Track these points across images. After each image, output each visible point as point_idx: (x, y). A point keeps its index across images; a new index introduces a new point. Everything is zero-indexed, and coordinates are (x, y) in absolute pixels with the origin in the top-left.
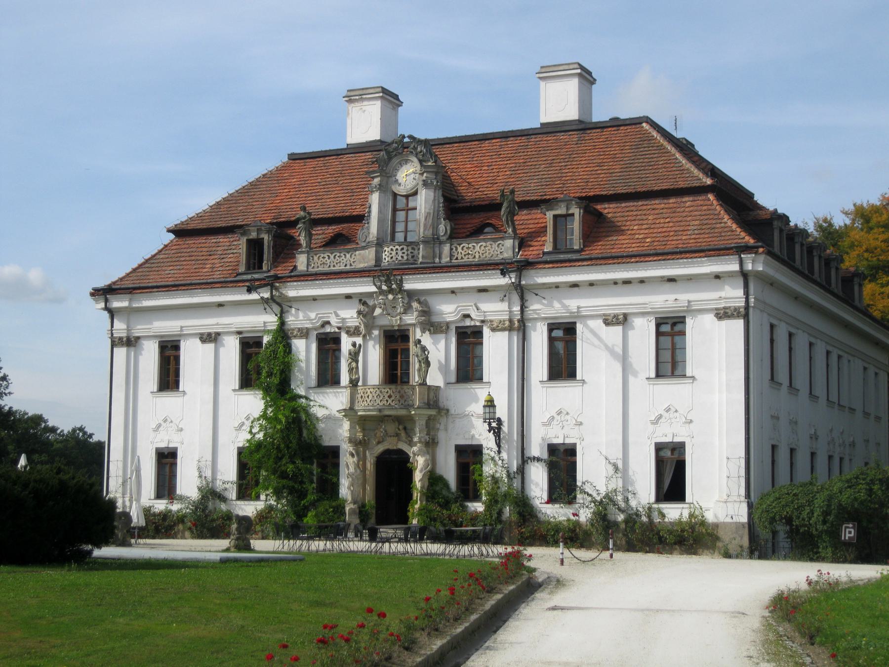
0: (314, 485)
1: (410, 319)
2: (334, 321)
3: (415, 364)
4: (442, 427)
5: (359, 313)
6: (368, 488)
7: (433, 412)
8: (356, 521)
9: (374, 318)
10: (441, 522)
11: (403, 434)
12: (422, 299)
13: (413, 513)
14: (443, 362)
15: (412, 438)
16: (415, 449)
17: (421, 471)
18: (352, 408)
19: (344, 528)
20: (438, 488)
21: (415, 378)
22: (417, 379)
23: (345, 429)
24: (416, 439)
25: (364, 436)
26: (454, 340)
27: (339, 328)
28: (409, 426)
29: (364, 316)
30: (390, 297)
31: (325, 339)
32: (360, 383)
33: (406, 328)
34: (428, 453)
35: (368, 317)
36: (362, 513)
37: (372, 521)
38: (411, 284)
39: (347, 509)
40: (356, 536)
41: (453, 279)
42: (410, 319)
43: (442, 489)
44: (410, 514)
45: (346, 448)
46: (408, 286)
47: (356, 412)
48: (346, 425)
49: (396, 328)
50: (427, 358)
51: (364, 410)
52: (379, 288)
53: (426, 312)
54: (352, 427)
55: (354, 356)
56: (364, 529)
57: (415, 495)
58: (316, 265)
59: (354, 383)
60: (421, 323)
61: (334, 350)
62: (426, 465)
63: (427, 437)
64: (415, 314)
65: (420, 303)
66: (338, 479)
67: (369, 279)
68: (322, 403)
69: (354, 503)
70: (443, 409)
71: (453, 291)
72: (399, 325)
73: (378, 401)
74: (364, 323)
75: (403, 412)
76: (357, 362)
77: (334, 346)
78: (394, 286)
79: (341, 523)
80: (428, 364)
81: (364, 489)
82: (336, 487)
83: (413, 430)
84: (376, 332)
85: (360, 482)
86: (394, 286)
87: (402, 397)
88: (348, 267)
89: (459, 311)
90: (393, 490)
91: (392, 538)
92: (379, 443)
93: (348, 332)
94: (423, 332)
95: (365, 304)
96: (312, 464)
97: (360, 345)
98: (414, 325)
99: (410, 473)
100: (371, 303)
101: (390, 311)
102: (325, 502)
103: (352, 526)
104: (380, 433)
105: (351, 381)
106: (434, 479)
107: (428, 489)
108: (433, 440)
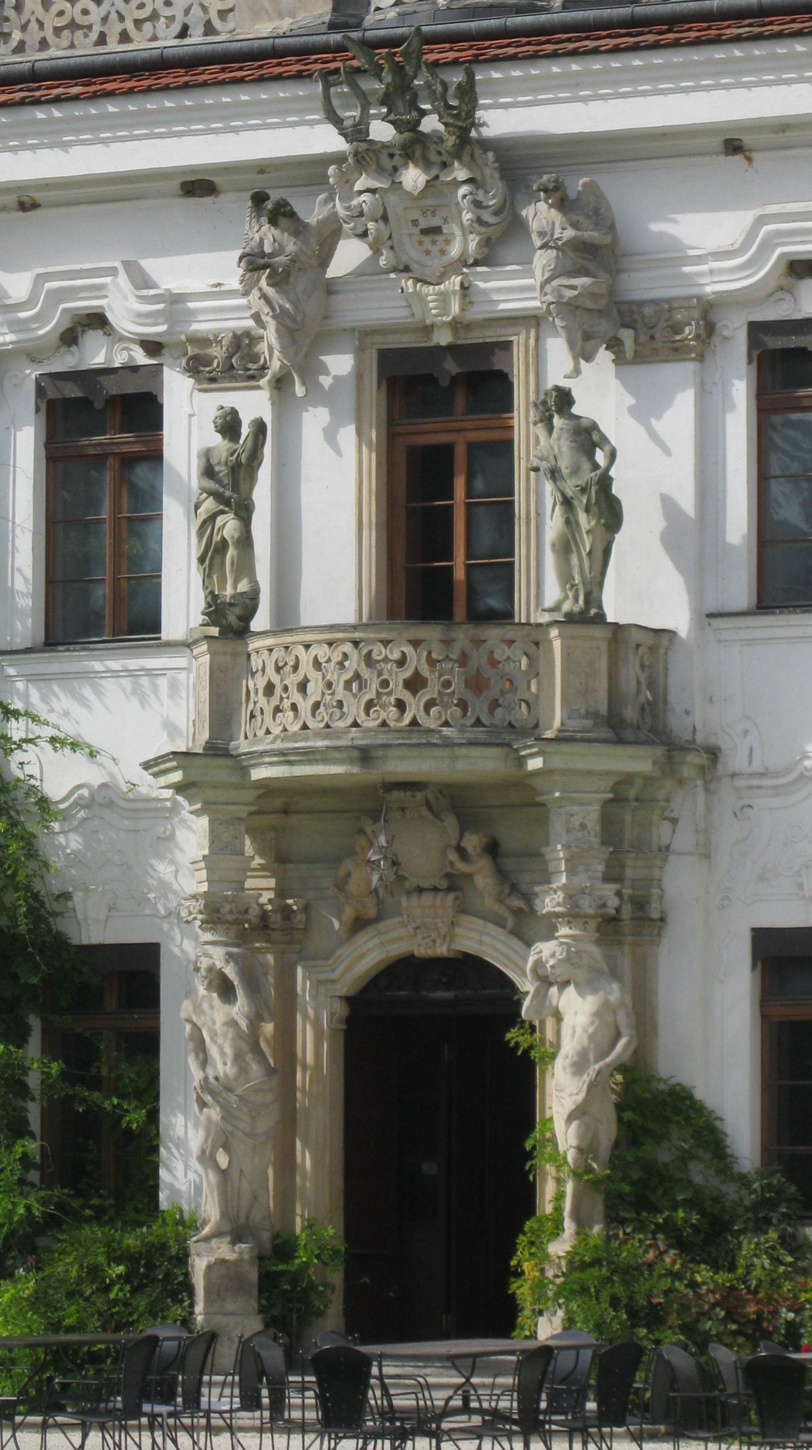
0: (33, 1146)
1: (517, 288)
2: (125, 309)
3: (541, 516)
4: (684, 839)
5: (255, 262)
6: (305, 1159)
7: (637, 761)
8: (243, 1321)
9: (330, 288)
10: (688, 1329)
11: (483, 878)
12: (577, 184)
13: (540, 1285)
14: (687, 503)
15: (529, 898)
16: (547, 951)
17: (579, 1066)
18: (217, 749)
19: (178, 1361)
20: (664, 1155)
21: (543, 588)
22: (552, 592)
23: (185, 857)
24: (551, 902)
25: (281, 892)
26: (740, 392)
27: (153, 347)
28: (512, 838)
29: (279, 280)
30: (413, 177)
31: (83, 404)
32: (261, 621)
33: (492, 335)
34: (615, 974)
35: (301, 284)
36: (276, 1284)
37: (327, 1331)
38: (521, 110)
39: (199, 1265)
40: (250, 1402)
41: (734, 76)
42: (517, 288)
43: (685, 1157)
44: (522, 1290)
45: (192, 952)
46: (499, 121)
47: (240, 765)
48: (193, 835)
49: (443, 338)
50: (605, 482)
51: (285, 757)
52: (356, 133)
53: (596, 252)
54: (221, 847)
55: (230, 482)
56: (293, 1363)
57: (547, 1191)
58: (34, 35)
59: (229, 621)
60: (570, 309)
61: (129, 461)
62: (606, 1034)
63: (608, 891)
64: (543, 260)
65: (563, 204)
66: (153, 1116)
67: (301, 90)
68: (68, 729)
69: (237, 1237)
70: (688, 747)
71: (734, 144)
72: (456, 325)
73: (354, 709)
74: (280, 316)
75: (484, 764)
76: (244, 511)
77: (126, 440)
78: (431, 124)
79: (167, 1333)
80: (610, 513)
81: (287, 1165)
82: (136, 1157)
83: (535, 856)
84: (340, 364)
85: (266, 1123)
86: (431, 124)
87: (477, 684)
88: (196, 38)
89: (767, 245)
90: (429, 1168)
91: (447, 1412)
92: (359, 924)
93: (197, 367)
94: (583, 352)
95: (282, 214)
96: (20, 1037)
97: (260, 428)
98: (531, 321)
99: (518, 1080)
100: (313, 212)
101: (412, 253)
102: (93, 1232)
103: (226, 1353)
104: (368, 876)
105: (216, 610)
106: (649, 1110)
107: (616, 1161)
108: (640, 904)
